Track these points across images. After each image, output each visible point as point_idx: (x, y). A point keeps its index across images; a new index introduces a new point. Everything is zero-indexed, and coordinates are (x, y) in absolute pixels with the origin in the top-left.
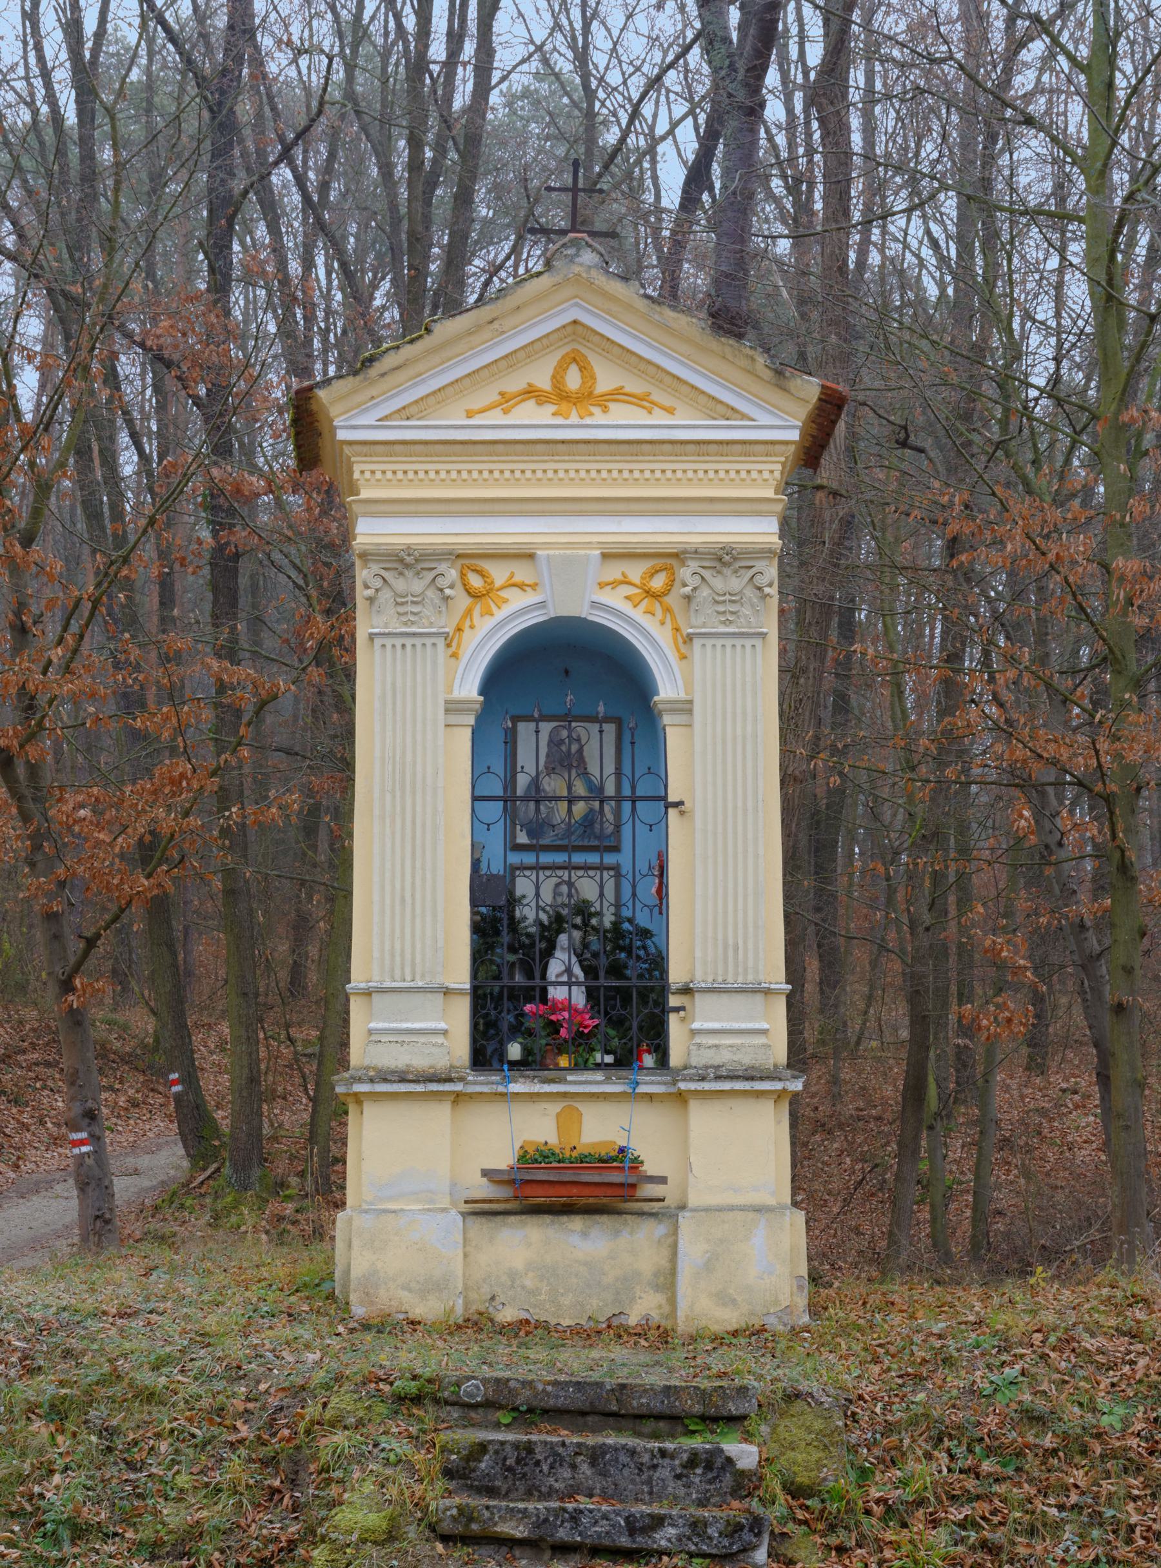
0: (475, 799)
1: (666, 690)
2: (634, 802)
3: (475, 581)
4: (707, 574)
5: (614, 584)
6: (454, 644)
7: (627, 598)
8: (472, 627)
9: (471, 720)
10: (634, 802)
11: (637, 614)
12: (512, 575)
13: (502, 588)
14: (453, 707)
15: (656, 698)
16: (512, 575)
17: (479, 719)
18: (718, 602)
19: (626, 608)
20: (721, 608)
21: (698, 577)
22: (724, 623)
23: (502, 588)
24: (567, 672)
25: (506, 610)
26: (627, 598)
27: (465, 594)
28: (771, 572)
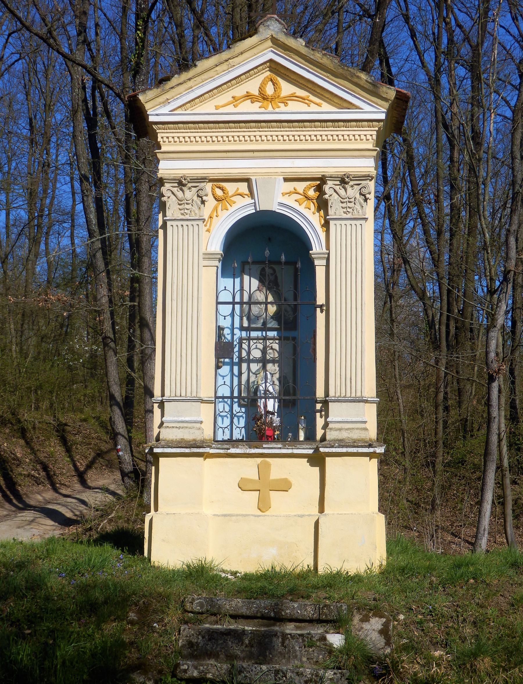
0: (218, 303)
1: (317, 249)
3: (219, 192)
4: (337, 188)
5: (290, 193)
6: (208, 225)
14: (209, 256)
15: (311, 252)
16: (238, 189)
22: (344, 212)
24: (269, 239)
25: (235, 207)
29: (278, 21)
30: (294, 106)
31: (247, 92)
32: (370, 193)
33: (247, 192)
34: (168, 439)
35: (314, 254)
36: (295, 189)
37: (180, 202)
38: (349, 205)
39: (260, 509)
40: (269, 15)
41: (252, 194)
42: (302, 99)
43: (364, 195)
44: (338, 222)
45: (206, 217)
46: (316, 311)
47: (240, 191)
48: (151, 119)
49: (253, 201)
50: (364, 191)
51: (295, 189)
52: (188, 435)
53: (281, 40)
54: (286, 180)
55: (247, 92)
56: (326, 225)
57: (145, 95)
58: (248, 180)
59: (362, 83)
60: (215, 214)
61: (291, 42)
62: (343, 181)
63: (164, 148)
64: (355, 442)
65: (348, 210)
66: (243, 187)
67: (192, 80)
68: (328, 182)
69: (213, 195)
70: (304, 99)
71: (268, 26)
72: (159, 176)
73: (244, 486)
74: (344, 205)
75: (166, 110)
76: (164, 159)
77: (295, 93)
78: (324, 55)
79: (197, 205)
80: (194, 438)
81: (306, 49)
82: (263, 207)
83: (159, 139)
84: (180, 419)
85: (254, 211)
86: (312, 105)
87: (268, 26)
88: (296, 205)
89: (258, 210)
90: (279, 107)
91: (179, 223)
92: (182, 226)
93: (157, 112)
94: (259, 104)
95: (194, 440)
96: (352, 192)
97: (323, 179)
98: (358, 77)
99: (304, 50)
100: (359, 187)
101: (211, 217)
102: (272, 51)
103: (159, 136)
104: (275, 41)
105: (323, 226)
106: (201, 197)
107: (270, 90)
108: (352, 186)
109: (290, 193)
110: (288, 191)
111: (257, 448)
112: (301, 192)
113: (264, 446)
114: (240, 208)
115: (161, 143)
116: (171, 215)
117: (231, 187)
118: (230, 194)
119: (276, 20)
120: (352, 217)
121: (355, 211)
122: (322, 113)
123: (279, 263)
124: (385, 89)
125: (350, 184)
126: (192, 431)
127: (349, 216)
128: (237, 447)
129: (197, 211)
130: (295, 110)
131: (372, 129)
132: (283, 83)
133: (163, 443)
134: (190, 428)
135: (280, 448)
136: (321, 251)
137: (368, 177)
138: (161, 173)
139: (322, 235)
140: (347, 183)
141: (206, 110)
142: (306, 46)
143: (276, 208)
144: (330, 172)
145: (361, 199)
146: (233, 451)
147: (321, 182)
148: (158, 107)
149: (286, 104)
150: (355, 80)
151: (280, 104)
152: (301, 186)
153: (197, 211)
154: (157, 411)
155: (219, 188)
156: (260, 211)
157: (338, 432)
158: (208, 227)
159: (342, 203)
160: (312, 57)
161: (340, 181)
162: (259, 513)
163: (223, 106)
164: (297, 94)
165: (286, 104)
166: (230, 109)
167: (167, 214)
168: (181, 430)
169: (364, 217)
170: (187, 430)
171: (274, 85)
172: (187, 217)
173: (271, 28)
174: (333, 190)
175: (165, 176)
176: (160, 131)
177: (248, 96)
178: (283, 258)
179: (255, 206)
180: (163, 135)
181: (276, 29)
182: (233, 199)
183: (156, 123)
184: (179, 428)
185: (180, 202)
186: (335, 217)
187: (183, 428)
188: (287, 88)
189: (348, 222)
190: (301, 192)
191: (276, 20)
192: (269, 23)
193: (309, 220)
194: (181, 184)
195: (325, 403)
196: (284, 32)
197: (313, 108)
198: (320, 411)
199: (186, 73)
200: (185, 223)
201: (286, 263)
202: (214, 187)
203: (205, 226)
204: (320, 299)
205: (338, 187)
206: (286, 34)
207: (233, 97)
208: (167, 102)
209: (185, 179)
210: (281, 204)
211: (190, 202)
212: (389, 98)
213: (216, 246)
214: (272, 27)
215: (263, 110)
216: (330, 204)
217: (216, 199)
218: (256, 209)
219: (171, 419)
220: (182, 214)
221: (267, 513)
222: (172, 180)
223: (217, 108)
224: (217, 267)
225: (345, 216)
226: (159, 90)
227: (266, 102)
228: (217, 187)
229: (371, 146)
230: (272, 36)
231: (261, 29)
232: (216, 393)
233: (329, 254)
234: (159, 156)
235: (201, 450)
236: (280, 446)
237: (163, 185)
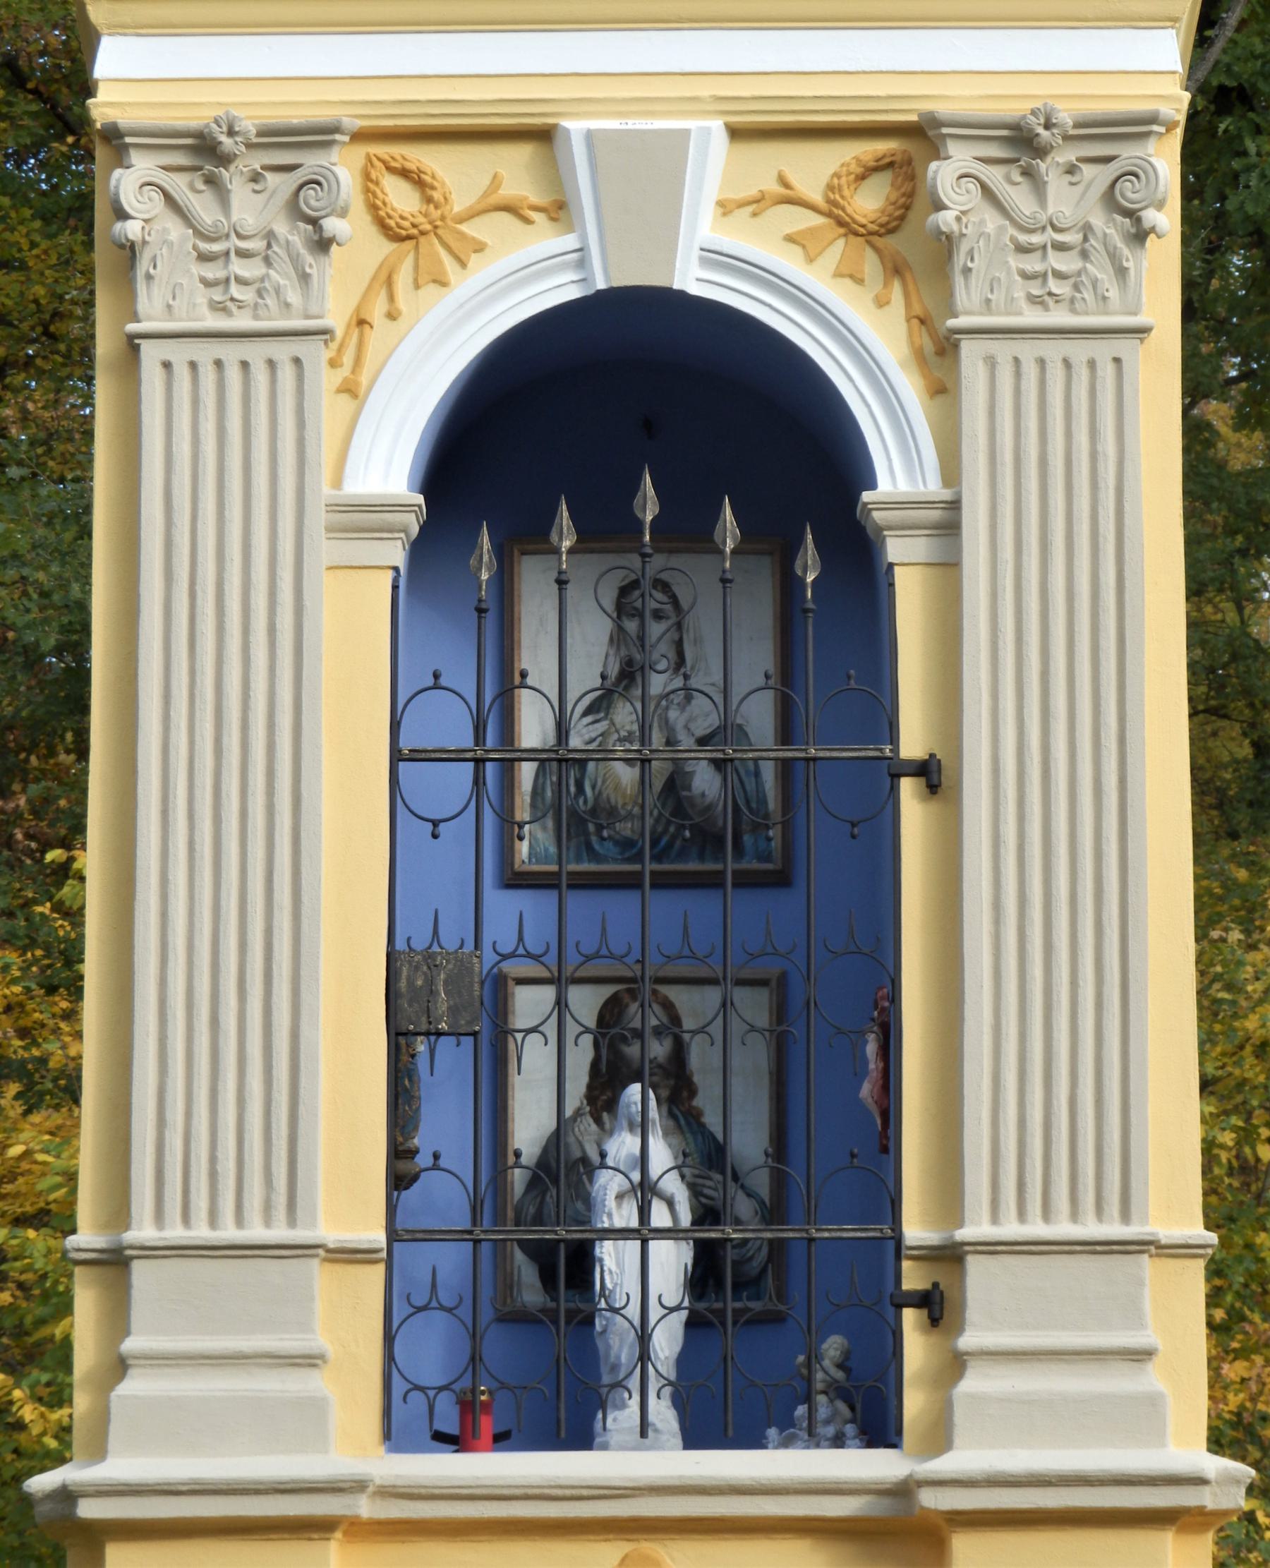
0: (396, 756)
1: (897, 473)
2: (644, 1243)
3: (401, 199)
4: (994, 176)
5: (759, 203)
6: (348, 359)
7: (790, 239)
8: (392, 316)
9: (397, 554)
10: (644, 1243)
11: (816, 279)
12: (496, 181)
13: (471, 215)
14: (359, 518)
15: (866, 496)
16: (496, 181)
17: (420, 549)
18: (1023, 249)
19: (789, 264)
20: (1033, 264)
21: (972, 186)
22: (1034, 300)
23: (471, 215)
24: (649, 427)
25: (483, 272)
26: (790, 239)
27: (373, 231)
28: (1165, 161)
32: (1160, 205)
37: (204, 246)
38: (1057, 261)
43: (1130, 214)
44: (1004, 350)
45: (336, 317)
46: (894, 791)
49: (570, 241)
50: (1129, 192)
58: (543, 136)
62: (1022, 142)
65: (235, 291)
66: (513, 168)
68: (953, 148)
69: (373, 208)
74: (1033, 264)
76: (122, 29)
79: (295, 260)
88: (789, 264)
91: (205, 352)
92: (219, 363)
96: (1069, 199)
97: (924, 135)
100: (1112, 170)
101: (361, 322)
106: (314, 222)
108: (255, 178)
109: (759, 203)
110: (753, 192)
112: (817, 197)
114: (513, 281)
117: (460, 174)
125: (239, 164)
127: (1059, 317)
129: (293, 297)
137: (1137, 127)
138: (104, 107)
140: (1041, 152)
143: (692, 280)
144: (952, 100)
145: (1110, 228)
153: (293, 297)
154: (86, 1301)
155: (404, 173)
158: (345, 371)
167: (143, 305)
172: (242, 322)
174: (158, 197)
175: (124, 119)
185: (204, 246)
189: (1053, 350)
190: (817, 197)
194: (205, 151)
200: (231, 353)
202: (378, 172)
203: (333, 363)
210: (715, 258)
211: (256, 245)
213: (386, 458)
220: (218, 308)
222: (975, 129)
224: (396, 569)
225: (1032, 317)
233: (954, 505)
237: (936, 152)
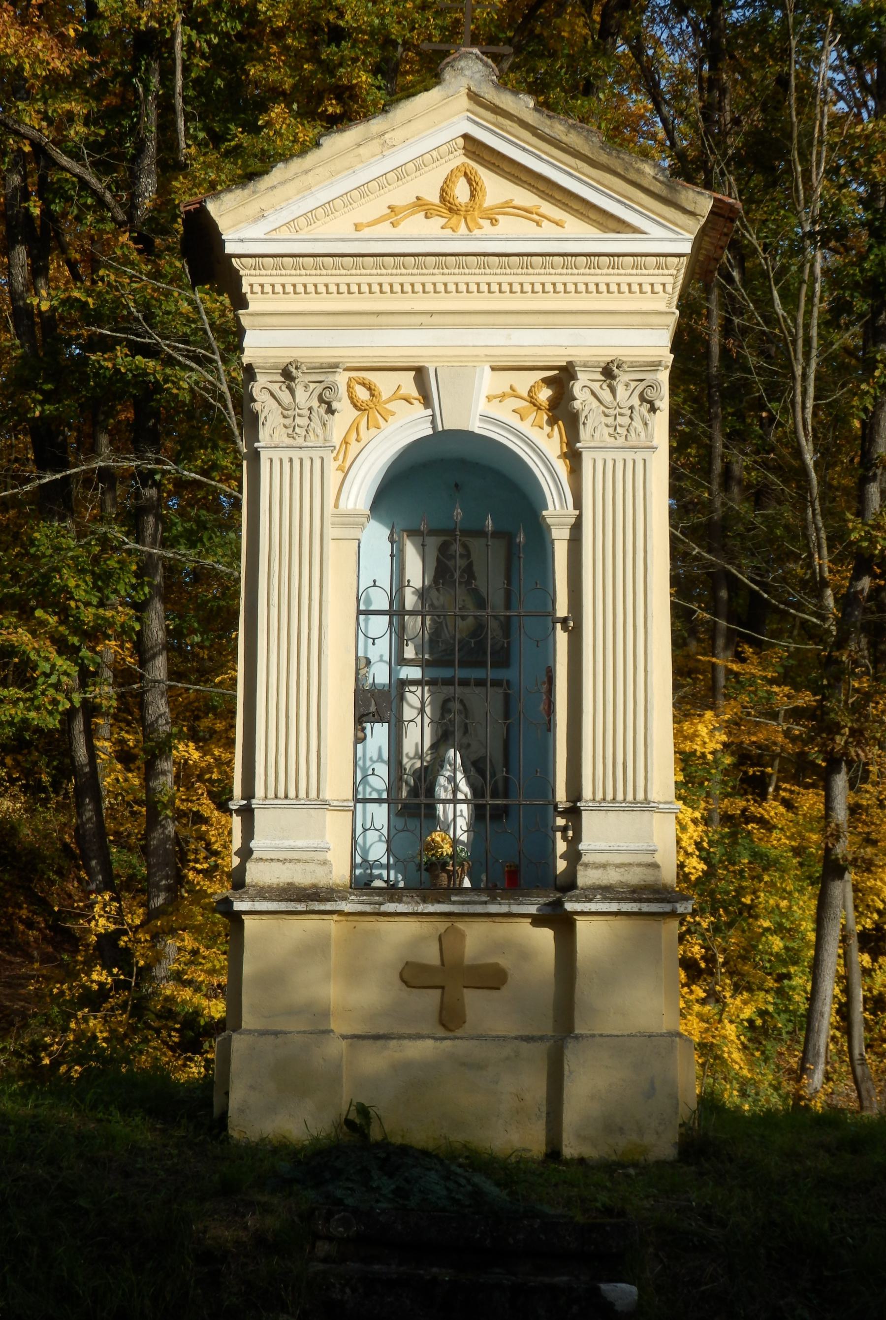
1: (556, 510)
3: (362, 394)
29: (481, 60)
30: (508, 225)
31: (418, 198)
33: (414, 393)
34: (261, 884)
35: (553, 516)
36: (511, 387)
39: (444, 1025)
40: (463, 49)
41: (427, 401)
42: (526, 212)
46: (554, 628)
47: (403, 391)
48: (229, 249)
51: (511, 387)
52: (302, 876)
53: (487, 96)
54: (493, 369)
55: (418, 198)
56: (573, 457)
57: (219, 202)
59: (645, 183)
60: (354, 435)
61: (506, 101)
63: (253, 306)
64: (634, 892)
67: (311, 173)
69: (351, 398)
70: (531, 213)
71: (462, 69)
72: (245, 360)
73: (381, 656)
75: (258, 230)
77: (512, 200)
78: (573, 126)
80: (314, 881)
81: (537, 115)
82: (451, 423)
83: (245, 289)
84: (287, 843)
85: (430, 432)
86: (545, 223)
87: (462, 69)
88: (514, 420)
89: (440, 429)
90: (480, 228)
93: (242, 235)
94: (442, 221)
95: (314, 886)
98: (638, 171)
99: (532, 118)
102: (469, 119)
103: (245, 281)
104: (473, 97)
105: (564, 456)
107: (461, 192)
109: (502, 397)
110: (500, 392)
111: (439, 902)
112: (525, 394)
113: (454, 898)
114: (407, 426)
115: (249, 296)
116: (267, 437)
117: (385, 383)
118: (384, 397)
119: (477, 57)
120: (627, 444)
121: (633, 434)
122: (567, 240)
123: (481, 533)
124: (691, 194)
126: (310, 867)
128: (400, 901)
130: (512, 234)
131: (666, 272)
132: (486, 176)
133: (252, 891)
134: (306, 862)
135: (485, 903)
136: (565, 512)
137: (655, 366)
139: (562, 468)
141: (336, 232)
142: (535, 109)
143: (477, 427)
144: (578, 354)
146: (390, 907)
147: (562, 379)
148: (245, 222)
149: (494, 222)
150: (632, 176)
151: (482, 222)
152: (525, 381)
153: (319, 431)
156: (444, 431)
157: (600, 871)
159: (606, 416)
160: (547, 131)
161: (602, 373)
162: (441, 1032)
163: (370, 225)
164: (516, 203)
165: (494, 222)
166: (384, 229)
168: (287, 864)
169: (649, 444)
170: (299, 867)
171: (470, 185)
173: (467, 73)
176: (247, 272)
177: (420, 204)
178: (489, 522)
179: (433, 422)
180: (253, 280)
181: (477, 76)
182: (388, 406)
183: (239, 256)
184: (284, 861)
186: (592, 444)
187: (291, 861)
188: (496, 189)
191: (477, 57)
192: (462, 63)
193: (538, 446)
195: (574, 813)
196: (492, 81)
197: (548, 229)
198: (564, 829)
199: (300, 160)
201: (496, 534)
204: (562, 610)
205: (598, 384)
206: (497, 86)
207: (389, 207)
208: (262, 216)
209: (297, 368)
210: (485, 418)
212: (698, 212)
214: (469, 72)
215: (448, 232)
216: (582, 419)
217: (355, 406)
218: (434, 427)
219: (268, 843)
221: (459, 1033)
223: (357, 227)
226: (246, 191)
227: (455, 218)
228: (359, 383)
229: (661, 306)
230: (469, 89)
231: (448, 74)
232: (356, 791)
234: (245, 321)
235: (328, 906)
236: (484, 898)
